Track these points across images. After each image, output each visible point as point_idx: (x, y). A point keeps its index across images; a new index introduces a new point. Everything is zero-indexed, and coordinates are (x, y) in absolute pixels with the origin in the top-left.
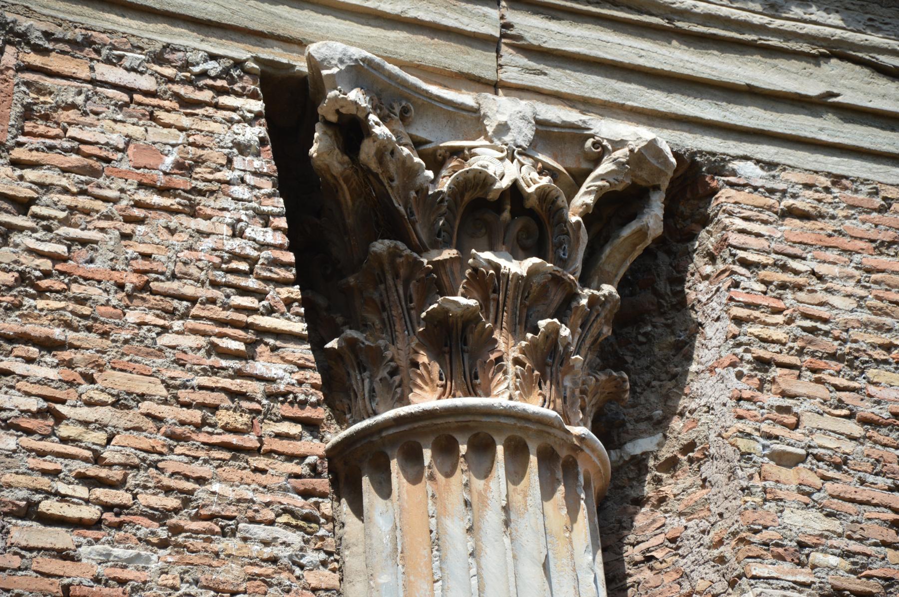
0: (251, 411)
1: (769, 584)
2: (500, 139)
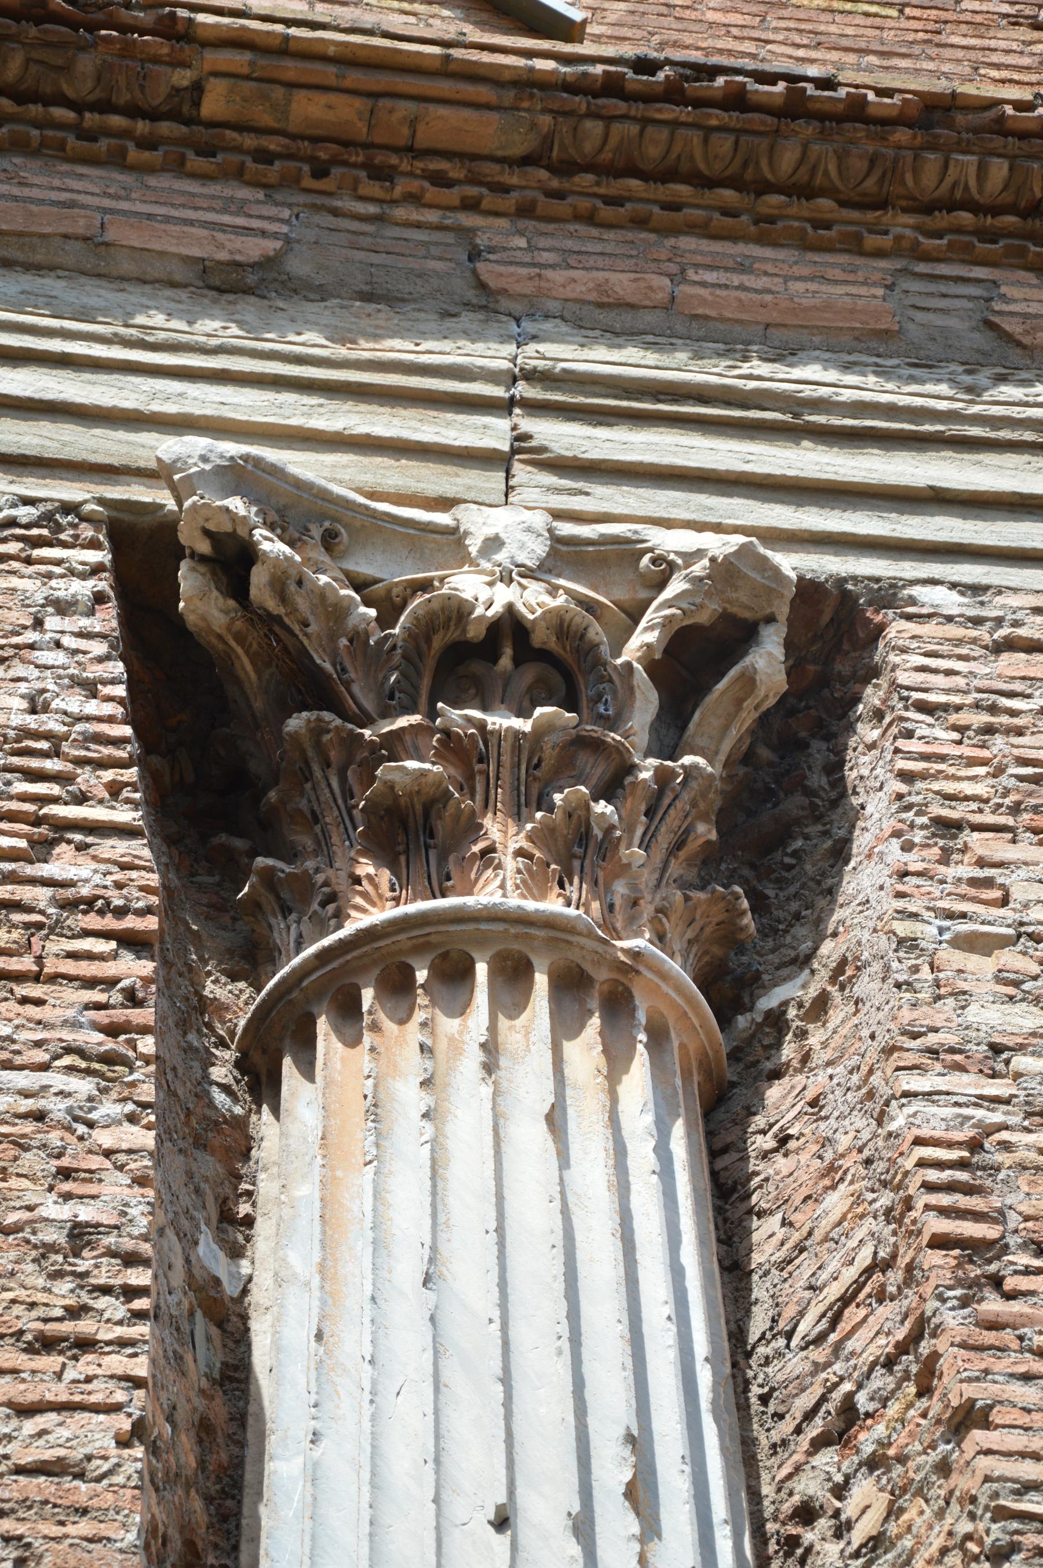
0: (27, 926)
1: (933, 1102)
2: (489, 560)
